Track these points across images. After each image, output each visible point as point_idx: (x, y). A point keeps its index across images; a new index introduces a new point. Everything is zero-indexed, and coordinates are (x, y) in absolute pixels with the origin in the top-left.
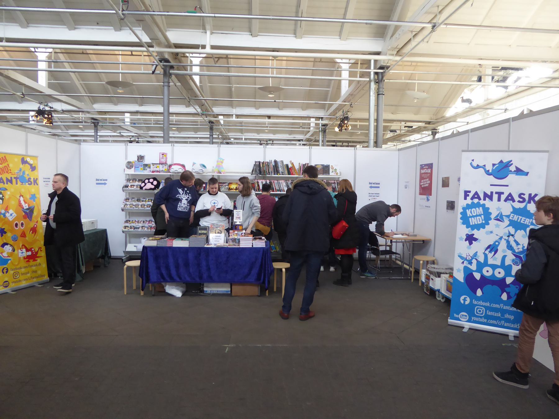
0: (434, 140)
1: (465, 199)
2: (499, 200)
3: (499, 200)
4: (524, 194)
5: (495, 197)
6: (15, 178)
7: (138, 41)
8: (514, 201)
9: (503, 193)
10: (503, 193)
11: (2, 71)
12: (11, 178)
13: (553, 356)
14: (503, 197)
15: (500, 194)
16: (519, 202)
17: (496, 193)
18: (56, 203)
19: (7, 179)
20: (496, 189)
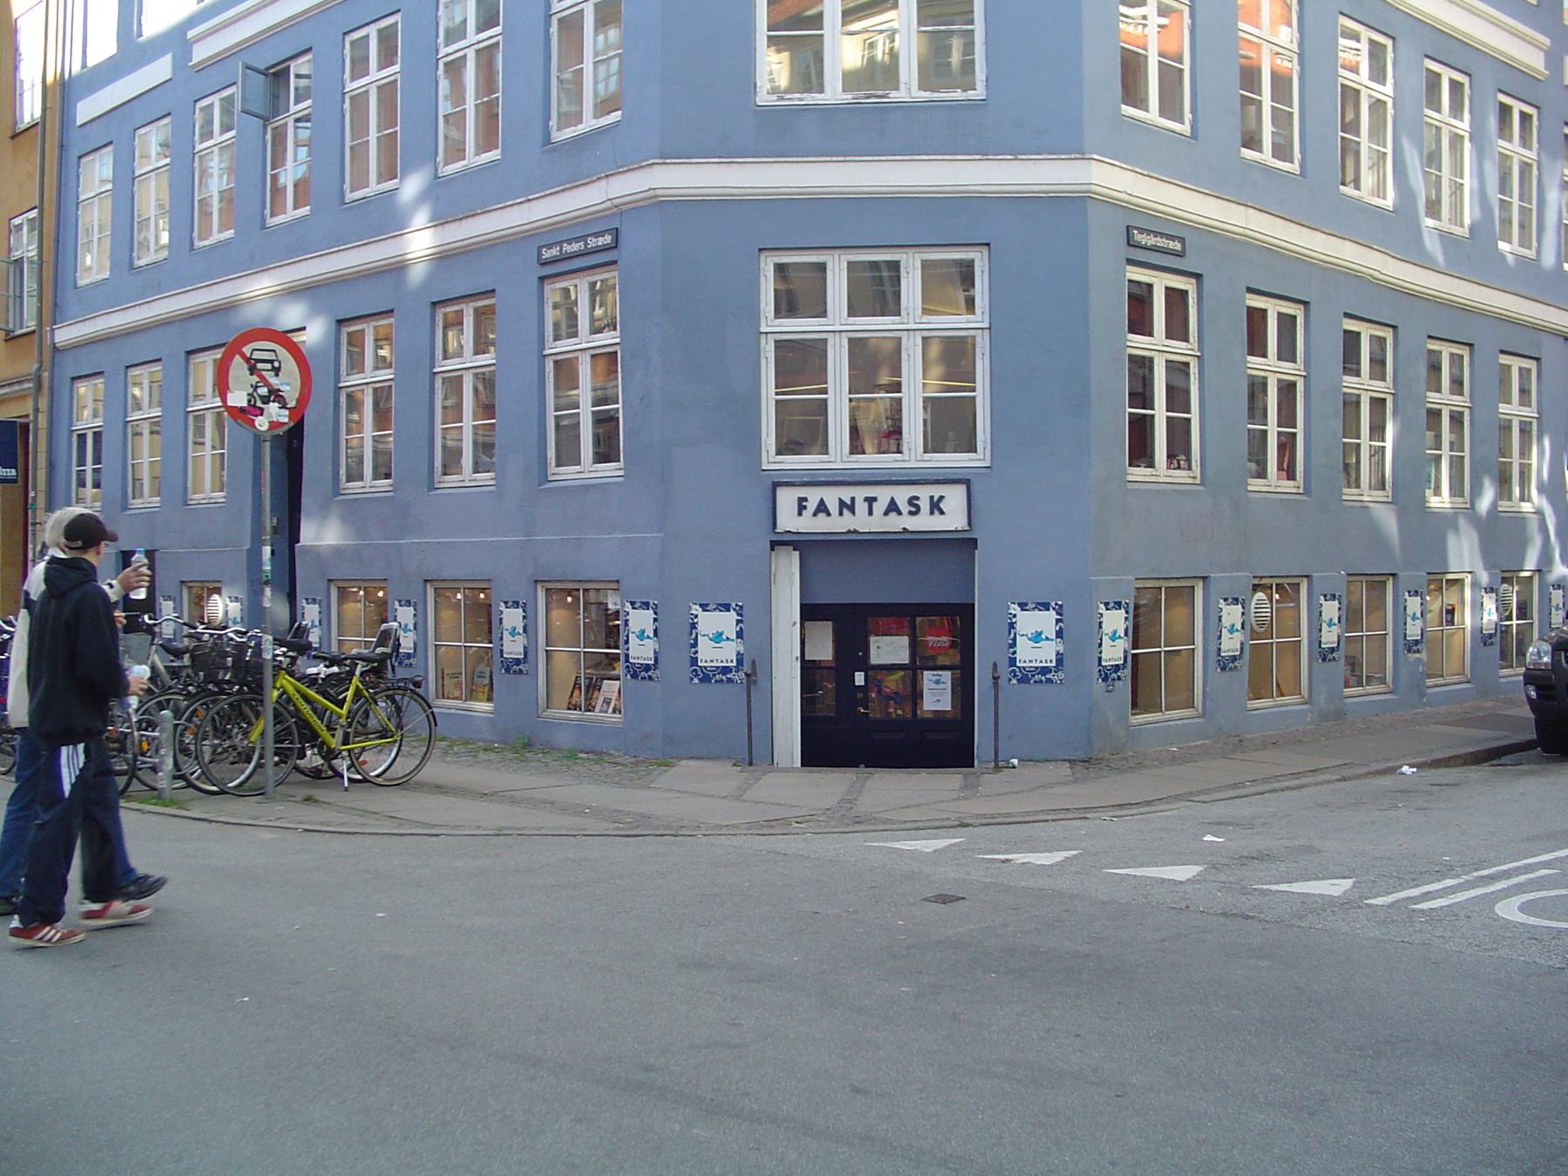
4: (917, 498)
5: (861, 507)
9: (875, 499)
10: (875, 499)
14: (880, 507)
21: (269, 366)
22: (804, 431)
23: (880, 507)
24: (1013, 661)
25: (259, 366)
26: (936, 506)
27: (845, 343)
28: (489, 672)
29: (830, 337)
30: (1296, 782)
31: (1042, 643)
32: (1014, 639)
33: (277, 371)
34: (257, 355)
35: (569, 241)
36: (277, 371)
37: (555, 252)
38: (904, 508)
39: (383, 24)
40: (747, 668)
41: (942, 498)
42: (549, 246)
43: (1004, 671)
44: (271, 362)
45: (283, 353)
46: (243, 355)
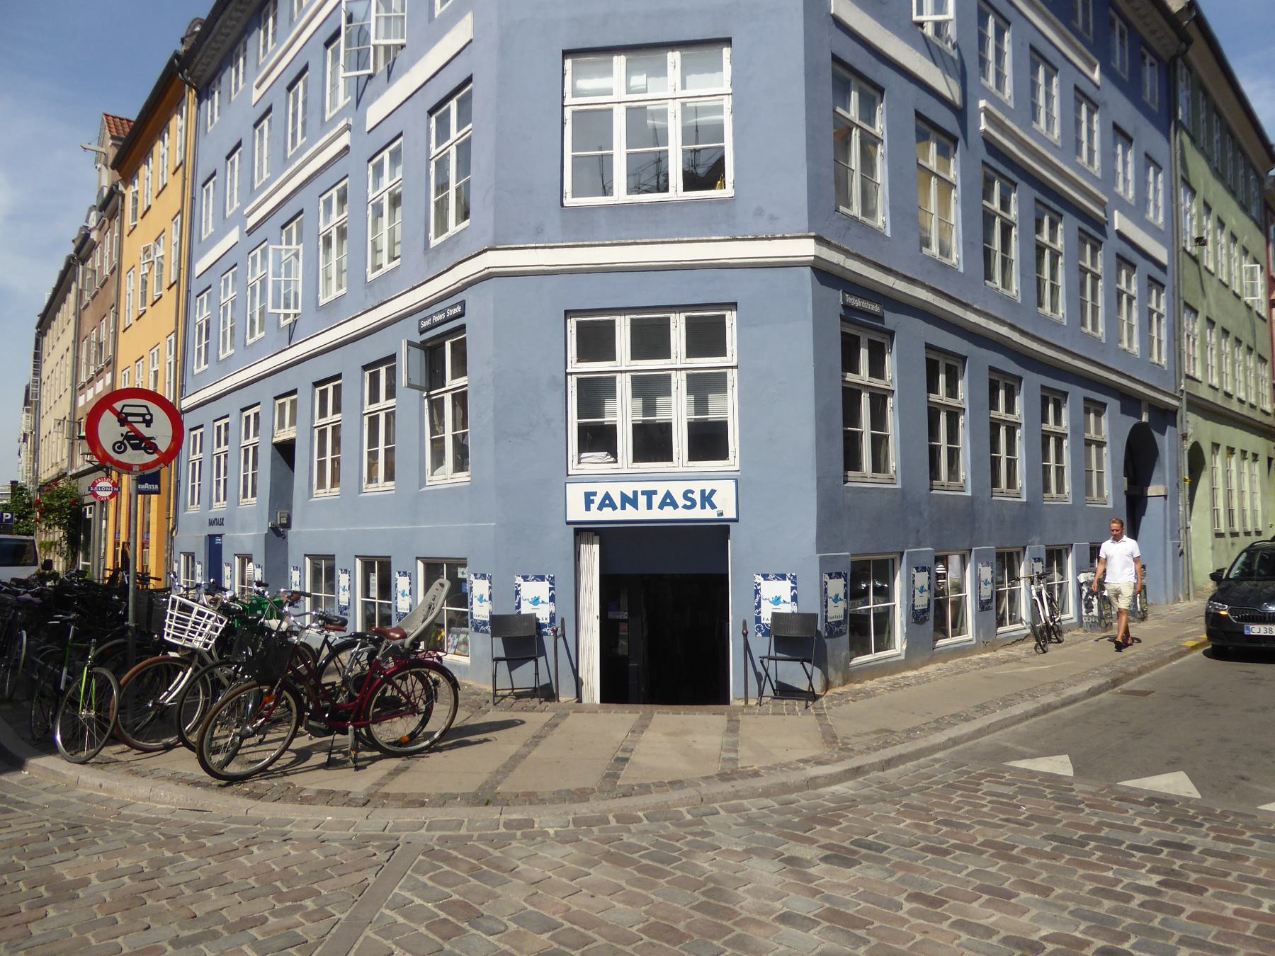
1: (588, 509)
2: (649, 506)
3: (649, 506)
4: (692, 492)
5: (642, 500)
6: (643, 493)
7: (958, 101)
8: (675, 506)
9: (655, 492)
10: (655, 492)
11: (271, 5)
12: (635, 493)
14: (657, 500)
15: (650, 494)
16: (685, 507)
17: (643, 493)
19: (623, 496)
21: (141, 419)
23: (657, 500)
24: (758, 620)
25: (130, 419)
26: (707, 499)
27: (684, 377)
29: (673, 373)
30: (1235, 494)
32: (759, 603)
33: (149, 423)
34: (126, 410)
35: (436, 314)
36: (149, 423)
37: (428, 323)
38: (681, 501)
40: (558, 624)
41: (713, 492)
42: (425, 319)
43: (752, 627)
44: (143, 415)
45: (155, 409)
46: (114, 411)
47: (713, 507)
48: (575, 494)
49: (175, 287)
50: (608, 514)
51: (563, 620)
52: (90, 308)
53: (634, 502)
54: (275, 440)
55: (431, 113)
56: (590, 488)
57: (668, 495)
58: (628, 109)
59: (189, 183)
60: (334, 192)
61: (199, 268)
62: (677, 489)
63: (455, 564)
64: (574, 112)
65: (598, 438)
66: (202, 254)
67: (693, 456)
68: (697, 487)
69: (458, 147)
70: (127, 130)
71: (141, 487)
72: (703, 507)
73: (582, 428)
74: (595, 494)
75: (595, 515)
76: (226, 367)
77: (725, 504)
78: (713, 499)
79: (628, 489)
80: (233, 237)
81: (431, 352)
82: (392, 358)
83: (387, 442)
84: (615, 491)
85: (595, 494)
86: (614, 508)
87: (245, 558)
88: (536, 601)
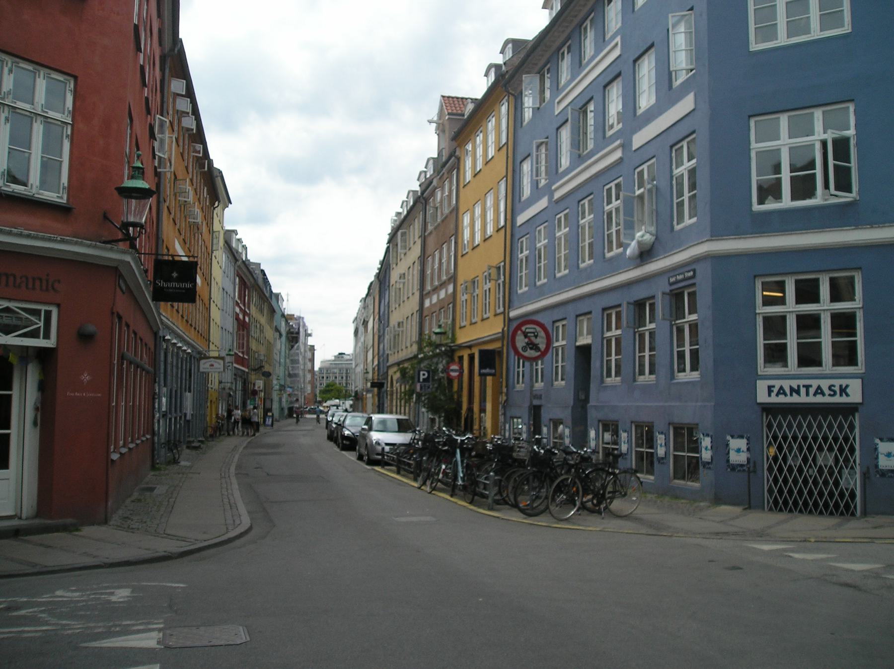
0: (419, 488)
1: (770, 395)
2: (807, 394)
3: (807, 394)
4: (834, 386)
5: (803, 391)
6: (804, 386)
8: (823, 394)
9: (811, 386)
10: (811, 386)
12: (799, 386)
13: (640, 129)
14: (812, 391)
15: (807, 387)
16: (830, 395)
17: (804, 386)
18: (129, 262)
20: (802, 382)
22: (776, 354)
23: (812, 391)
26: (843, 390)
28: (648, 461)
31: (741, 453)
32: (877, 456)
38: (827, 392)
39: (616, 182)
41: (847, 386)
47: (847, 395)
48: (762, 386)
49: (503, 230)
50: (781, 399)
51: (755, 463)
52: (433, 235)
53: (798, 392)
54: (578, 344)
55: (672, 147)
56: (771, 382)
57: (819, 387)
58: (790, 148)
59: (510, 155)
60: (613, 185)
61: (521, 219)
62: (825, 384)
63: (691, 430)
64: (757, 153)
65: (776, 354)
66: (523, 210)
67: (836, 363)
68: (837, 383)
69: (689, 171)
70: (479, 139)
71: (483, 371)
72: (841, 395)
73: (784, 335)
74: (774, 387)
75: (774, 399)
76: (541, 292)
77: (855, 395)
78: (847, 390)
79: (794, 384)
80: (543, 203)
81: (676, 296)
82: (653, 297)
83: (651, 349)
84: (786, 384)
85: (774, 387)
86: (786, 395)
87: (556, 423)
88: (738, 450)
